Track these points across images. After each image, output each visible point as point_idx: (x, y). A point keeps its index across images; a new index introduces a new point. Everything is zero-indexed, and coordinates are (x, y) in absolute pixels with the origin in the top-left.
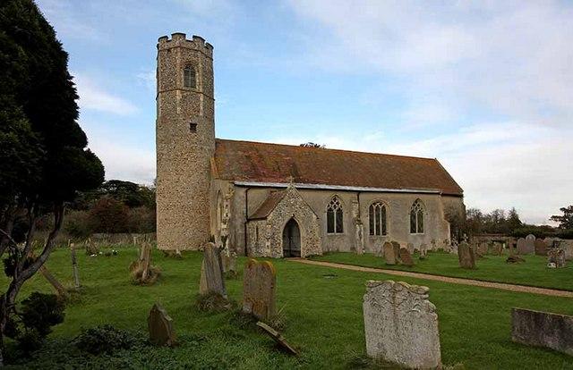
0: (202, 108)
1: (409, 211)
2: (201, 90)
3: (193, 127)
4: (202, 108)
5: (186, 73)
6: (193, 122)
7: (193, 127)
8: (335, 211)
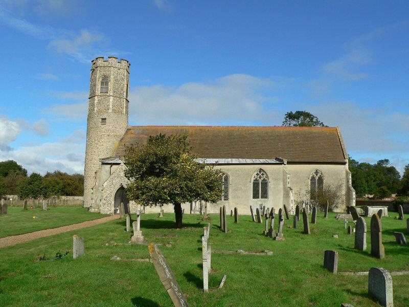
0: (111, 106)
1: (253, 179)
2: (112, 94)
3: (104, 120)
4: (111, 106)
5: (102, 83)
6: (103, 117)
7: (104, 120)
8: (260, 181)
